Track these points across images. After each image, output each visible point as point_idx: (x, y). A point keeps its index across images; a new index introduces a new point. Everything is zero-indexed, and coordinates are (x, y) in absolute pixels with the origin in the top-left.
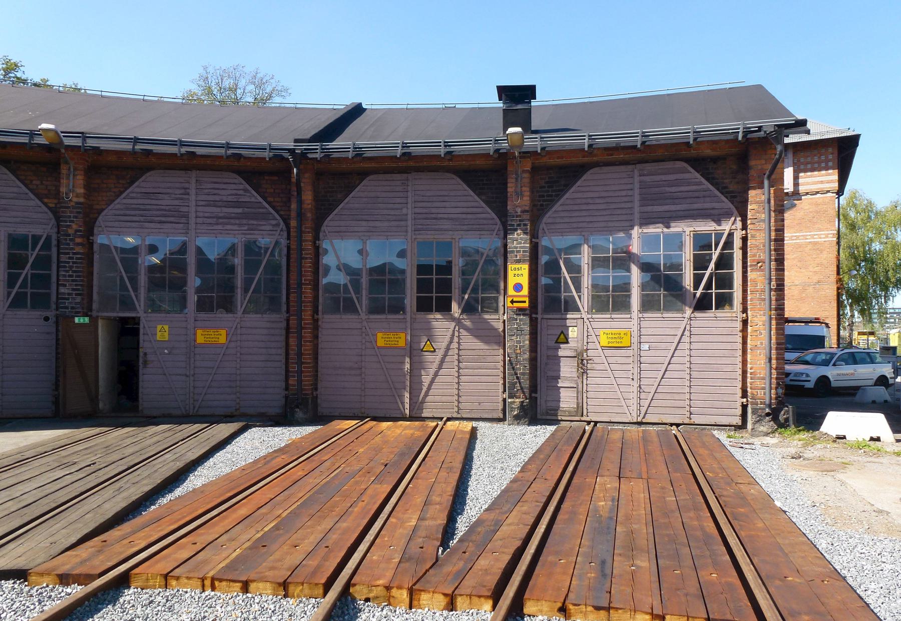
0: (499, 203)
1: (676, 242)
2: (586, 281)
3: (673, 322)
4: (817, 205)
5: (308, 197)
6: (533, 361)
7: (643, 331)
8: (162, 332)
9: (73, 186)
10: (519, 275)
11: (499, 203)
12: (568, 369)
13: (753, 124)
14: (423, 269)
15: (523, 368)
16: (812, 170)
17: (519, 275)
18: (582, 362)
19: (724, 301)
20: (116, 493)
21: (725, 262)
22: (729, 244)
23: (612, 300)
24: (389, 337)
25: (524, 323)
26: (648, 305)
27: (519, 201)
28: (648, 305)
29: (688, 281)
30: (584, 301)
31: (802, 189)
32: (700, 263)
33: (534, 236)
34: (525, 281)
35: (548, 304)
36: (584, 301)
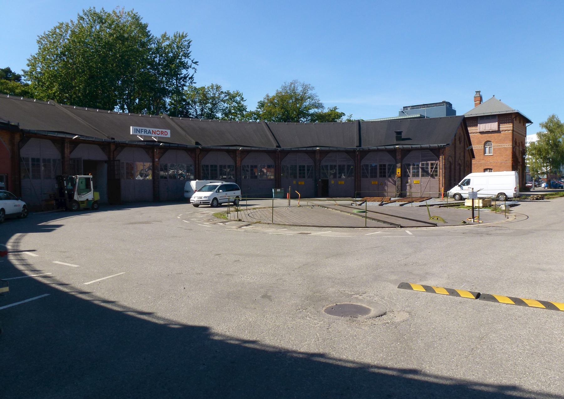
0: (395, 157)
1: (427, 164)
2: (411, 171)
3: (427, 179)
4: (506, 135)
5: (359, 157)
6: (401, 186)
7: (236, 219)
8: (333, 182)
9: (318, 157)
10: (399, 171)
11: (395, 157)
12: (408, 188)
13: (440, 145)
14: (381, 166)
15: (400, 187)
16: (504, 123)
17: (399, 171)
18: (410, 186)
19: (436, 175)
20: (514, 140)
21: (436, 168)
22: (437, 165)
23: (416, 175)
24: (374, 182)
25: (400, 179)
26: (423, 176)
27: (399, 157)
28: (423, 176)
29: (430, 172)
30: (411, 175)
31: (501, 129)
32: (432, 168)
33: (401, 163)
34: (400, 172)
35: (404, 175)
36: (411, 175)
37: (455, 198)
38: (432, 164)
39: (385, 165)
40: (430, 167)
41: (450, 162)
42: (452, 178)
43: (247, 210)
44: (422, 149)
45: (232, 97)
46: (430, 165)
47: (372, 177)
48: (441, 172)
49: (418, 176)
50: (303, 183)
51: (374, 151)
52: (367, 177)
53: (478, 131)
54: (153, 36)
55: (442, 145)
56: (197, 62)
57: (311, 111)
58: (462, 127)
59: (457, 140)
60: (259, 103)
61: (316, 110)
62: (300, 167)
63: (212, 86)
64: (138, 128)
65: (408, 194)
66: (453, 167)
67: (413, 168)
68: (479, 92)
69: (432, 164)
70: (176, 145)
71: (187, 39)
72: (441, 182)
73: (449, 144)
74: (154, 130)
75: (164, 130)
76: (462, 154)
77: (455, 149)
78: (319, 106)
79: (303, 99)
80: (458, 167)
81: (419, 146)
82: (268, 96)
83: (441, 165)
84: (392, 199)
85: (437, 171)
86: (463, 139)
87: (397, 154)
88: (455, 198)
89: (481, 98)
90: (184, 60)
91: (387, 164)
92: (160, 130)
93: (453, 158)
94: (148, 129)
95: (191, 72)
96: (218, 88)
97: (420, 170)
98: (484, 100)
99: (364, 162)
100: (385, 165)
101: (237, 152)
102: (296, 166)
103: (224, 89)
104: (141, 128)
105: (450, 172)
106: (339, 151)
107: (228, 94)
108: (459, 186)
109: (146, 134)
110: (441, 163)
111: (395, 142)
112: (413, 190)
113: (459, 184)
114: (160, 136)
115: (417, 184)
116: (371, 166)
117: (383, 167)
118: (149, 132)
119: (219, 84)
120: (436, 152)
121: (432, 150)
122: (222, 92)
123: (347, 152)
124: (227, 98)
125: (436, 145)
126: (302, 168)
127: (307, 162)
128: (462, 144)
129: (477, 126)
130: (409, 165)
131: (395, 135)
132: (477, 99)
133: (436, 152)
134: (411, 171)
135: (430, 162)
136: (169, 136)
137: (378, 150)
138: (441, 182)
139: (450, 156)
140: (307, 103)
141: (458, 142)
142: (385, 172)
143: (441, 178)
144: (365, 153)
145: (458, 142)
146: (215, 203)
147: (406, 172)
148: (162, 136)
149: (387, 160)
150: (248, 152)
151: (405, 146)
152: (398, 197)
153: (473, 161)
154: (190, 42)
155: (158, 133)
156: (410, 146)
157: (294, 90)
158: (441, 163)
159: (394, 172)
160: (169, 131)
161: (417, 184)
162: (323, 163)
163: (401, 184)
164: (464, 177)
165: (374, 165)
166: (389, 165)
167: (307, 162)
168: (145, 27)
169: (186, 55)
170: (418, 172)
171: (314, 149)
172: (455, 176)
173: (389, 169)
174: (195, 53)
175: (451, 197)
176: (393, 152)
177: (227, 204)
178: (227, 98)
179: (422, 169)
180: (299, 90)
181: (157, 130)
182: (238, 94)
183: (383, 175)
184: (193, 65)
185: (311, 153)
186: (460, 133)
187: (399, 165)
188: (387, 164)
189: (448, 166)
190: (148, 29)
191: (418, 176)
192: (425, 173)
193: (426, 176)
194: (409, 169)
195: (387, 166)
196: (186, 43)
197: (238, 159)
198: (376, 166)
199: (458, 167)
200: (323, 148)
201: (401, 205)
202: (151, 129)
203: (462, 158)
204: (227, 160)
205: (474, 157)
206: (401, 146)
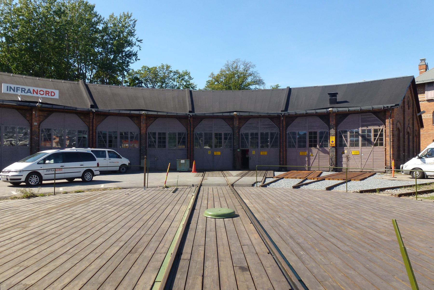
0: (328, 123)
1: (369, 131)
3: (368, 149)
5: (284, 123)
6: (336, 158)
8: (254, 152)
9: (236, 123)
10: (333, 139)
11: (328, 123)
12: (344, 160)
13: (386, 106)
15: (334, 160)
17: (333, 139)
19: (381, 144)
21: (381, 135)
23: (355, 144)
25: (334, 149)
26: (363, 145)
27: (333, 122)
28: (363, 145)
29: (372, 140)
30: (348, 144)
32: (375, 136)
33: (336, 130)
34: (334, 140)
35: (340, 145)
36: (348, 144)
37: (413, 175)
38: (376, 131)
39: (315, 133)
40: (372, 134)
41: (399, 129)
42: (401, 149)
43: (55, 194)
44: (362, 112)
45: (181, 77)
46: (372, 131)
47: (300, 146)
48: (388, 140)
49: (357, 145)
50: (219, 153)
51: (302, 116)
52: (294, 146)
53: (426, 99)
54: (100, 16)
55: (389, 105)
56: (141, 40)
57: (253, 87)
58: (411, 90)
59: (406, 103)
60: (207, 82)
61: (257, 86)
62: (216, 134)
63: (163, 66)
64: (13, 86)
65: (344, 166)
66: (401, 134)
67: (351, 136)
68: (424, 60)
69: (376, 131)
70: (63, 107)
71: (132, 18)
72: (388, 153)
73: (398, 105)
74: (36, 89)
75: (50, 90)
76: (411, 121)
77: (404, 114)
78: (259, 82)
79: (245, 78)
80: (406, 136)
81: (358, 108)
82: (212, 74)
83: (388, 131)
84: (325, 174)
85: (382, 140)
86: (411, 105)
87: (331, 120)
88: (413, 175)
89: (427, 66)
90: (130, 38)
91: (319, 131)
92: (45, 90)
93: (402, 124)
94: (27, 88)
95: (134, 49)
96: (168, 67)
97: (360, 138)
98: (430, 67)
99: (290, 130)
100: (315, 133)
101: (142, 118)
102: (212, 134)
103: (173, 69)
104: (16, 86)
105: (399, 140)
106: (260, 117)
107: (176, 73)
108: (420, 158)
109: (23, 94)
110: (387, 129)
111: (329, 105)
112: (351, 162)
113: (420, 155)
114: (44, 96)
115: (356, 156)
116: (299, 134)
117: (313, 135)
118: (29, 91)
119: (169, 65)
120: (381, 115)
121: (375, 112)
122: (171, 71)
123: (271, 117)
124: (176, 77)
125: (381, 106)
126: (219, 136)
127: (225, 129)
128: (411, 110)
129: (424, 93)
130: (346, 132)
131: (328, 97)
132: (422, 68)
133: (381, 115)
134: (348, 139)
135: (372, 128)
136: (57, 96)
137: (307, 115)
138: (388, 153)
139: (398, 121)
140: (249, 79)
141: (406, 107)
142: (316, 140)
143: (388, 148)
144: (291, 118)
145: (406, 107)
146: (34, 180)
147: (341, 140)
148: (47, 96)
149: (318, 126)
150: (156, 117)
151: (340, 109)
152: (333, 171)
153: (422, 131)
154: (135, 22)
155: (42, 93)
156: (347, 109)
157: (236, 67)
158: (387, 129)
159: (327, 139)
160: (57, 92)
161: (356, 156)
162: (243, 131)
163: (336, 155)
164: (428, 145)
165: (302, 133)
166: (321, 133)
167: (225, 129)
168: (92, 8)
169: (131, 34)
170: (358, 141)
171: (232, 114)
172: (404, 146)
173: (321, 138)
174: (139, 33)
175: (406, 174)
176: (325, 117)
177: (53, 181)
178: (176, 77)
179: (363, 137)
180: (241, 68)
181: (39, 89)
182: (187, 73)
183: (313, 144)
184: (138, 43)
185: (229, 119)
186: (409, 97)
187: (333, 131)
188: (319, 131)
189: (396, 133)
190: (95, 10)
191: (357, 145)
192: (367, 141)
193: (368, 146)
194: (346, 137)
195: (318, 134)
196: (131, 23)
197: (143, 125)
198: (305, 134)
199: (406, 136)
200: (241, 114)
201: (329, 189)
202: (32, 89)
203: (411, 126)
204: (131, 127)
205: (422, 126)
206: (335, 110)
